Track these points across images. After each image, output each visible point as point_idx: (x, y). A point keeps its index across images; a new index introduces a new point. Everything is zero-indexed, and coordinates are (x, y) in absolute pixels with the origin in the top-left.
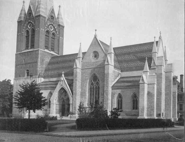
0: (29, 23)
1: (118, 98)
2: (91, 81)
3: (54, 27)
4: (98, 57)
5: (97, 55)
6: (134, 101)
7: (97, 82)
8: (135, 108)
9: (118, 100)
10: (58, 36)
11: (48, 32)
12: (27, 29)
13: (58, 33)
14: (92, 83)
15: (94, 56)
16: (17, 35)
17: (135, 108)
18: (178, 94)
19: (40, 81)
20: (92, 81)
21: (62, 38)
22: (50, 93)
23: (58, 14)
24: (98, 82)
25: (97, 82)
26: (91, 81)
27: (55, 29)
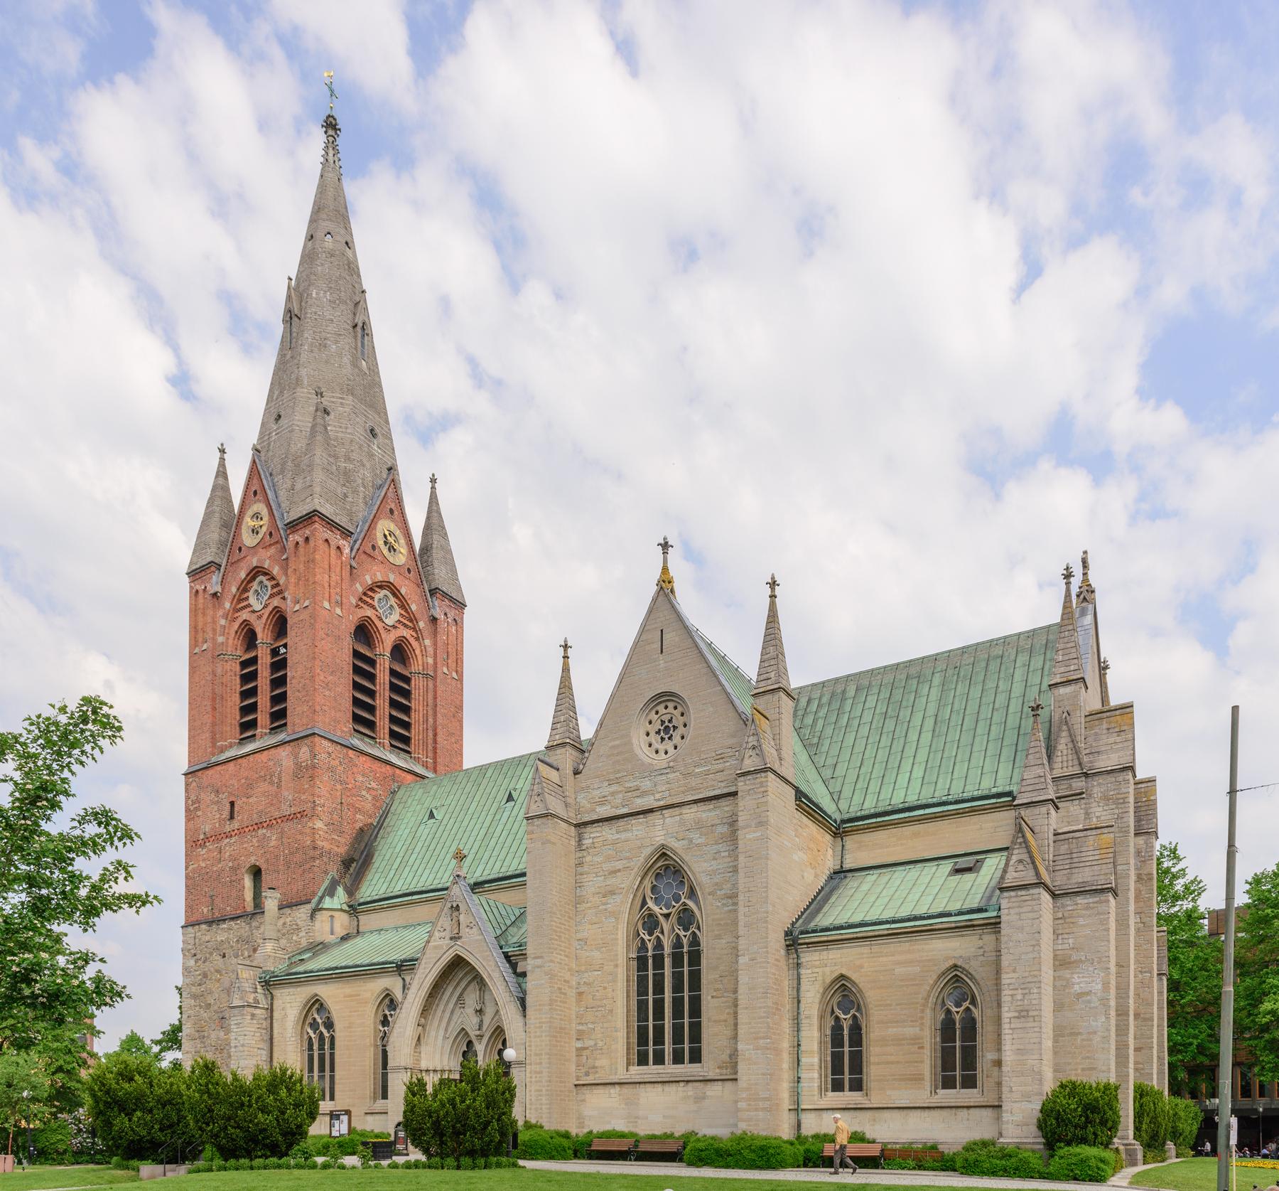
0: (253, 579)
1: (827, 1011)
2: (644, 903)
3: (404, 605)
4: (681, 730)
5: (675, 723)
6: (947, 1029)
7: (684, 904)
8: (650, 961)
9: (830, 1022)
10: (430, 661)
11: (364, 632)
12: (244, 615)
13: (427, 642)
14: (651, 915)
15: (658, 732)
16: (192, 655)
17: (650, 961)
18: (1235, 957)
19: (857, 799)
20: (650, 904)
21: (454, 675)
22: (387, 1001)
23: (428, 529)
24: (691, 904)
25: (686, 910)
26: (644, 903)
27: (410, 619)
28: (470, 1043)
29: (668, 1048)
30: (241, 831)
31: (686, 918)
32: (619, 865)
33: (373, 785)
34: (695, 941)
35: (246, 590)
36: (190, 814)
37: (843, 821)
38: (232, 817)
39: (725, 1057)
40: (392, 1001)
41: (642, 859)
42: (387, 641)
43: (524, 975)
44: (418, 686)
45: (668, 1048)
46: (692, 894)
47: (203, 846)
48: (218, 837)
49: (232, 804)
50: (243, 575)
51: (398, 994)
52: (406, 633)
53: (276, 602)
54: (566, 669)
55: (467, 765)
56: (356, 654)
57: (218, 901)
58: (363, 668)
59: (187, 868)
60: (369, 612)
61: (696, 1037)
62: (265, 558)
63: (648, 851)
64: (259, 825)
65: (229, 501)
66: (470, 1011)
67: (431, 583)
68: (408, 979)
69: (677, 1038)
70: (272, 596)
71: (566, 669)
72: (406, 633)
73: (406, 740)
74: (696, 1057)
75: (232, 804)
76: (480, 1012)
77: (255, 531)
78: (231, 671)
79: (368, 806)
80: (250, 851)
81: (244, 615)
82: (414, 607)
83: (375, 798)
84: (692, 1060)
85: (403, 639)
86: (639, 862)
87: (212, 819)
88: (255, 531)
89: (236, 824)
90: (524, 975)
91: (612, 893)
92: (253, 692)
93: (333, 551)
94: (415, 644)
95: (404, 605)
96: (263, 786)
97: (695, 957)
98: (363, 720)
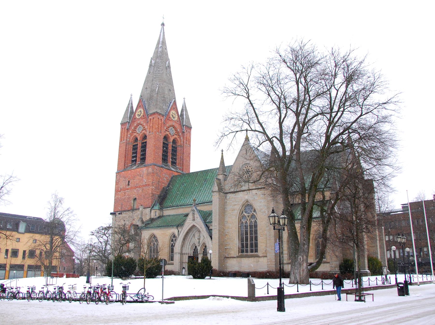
10: (182, 142)
12: (135, 134)
13: (182, 138)
23: (182, 111)
24: (255, 213)
28: (196, 247)
29: (249, 249)
30: (131, 188)
31: (253, 216)
32: (236, 203)
33: (167, 176)
34: (256, 222)
35: (136, 128)
36: (117, 183)
37: (344, 110)
38: (129, 185)
39: (264, 251)
40: (174, 235)
41: (242, 202)
42: (171, 139)
43: (211, 230)
44: (179, 149)
45: (249, 249)
46: (255, 211)
47: (120, 191)
48: (124, 189)
49: (129, 181)
50: (135, 125)
51: (176, 234)
52: (176, 136)
53: (144, 131)
54: (222, 156)
55: (192, 171)
56: (164, 143)
57: (123, 206)
58: (165, 145)
59: (115, 197)
60: (167, 133)
61: (256, 246)
62: (142, 122)
63: (243, 200)
64: (136, 187)
65: (132, 107)
66: (196, 239)
67: (184, 127)
68: (180, 230)
69: (252, 246)
70: (143, 130)
71: (222, 156)
72: (176, 136)
73: (175, 163)
74: (256, 251)
75: (129, 181)
76: (199, 239)
77: (139, 115)
78: (130, 147)
79: (166, 182)
80: (134, 193)
81: (135, 134)
82: (179, 130)
83: (167, 179)
84: (255, 252)
85: (176, 138)
86: (241, 203)
87: (123, 184)
88: (139, 115)
89: (130, 187)
90: (211, 230)
91: (234, 210)
92: (136, 153)
93: (160, 120)
94: (178, 139)
95: (176, 130)
96: (138, 177)
97: (256, 226)
98: (165, 159)
